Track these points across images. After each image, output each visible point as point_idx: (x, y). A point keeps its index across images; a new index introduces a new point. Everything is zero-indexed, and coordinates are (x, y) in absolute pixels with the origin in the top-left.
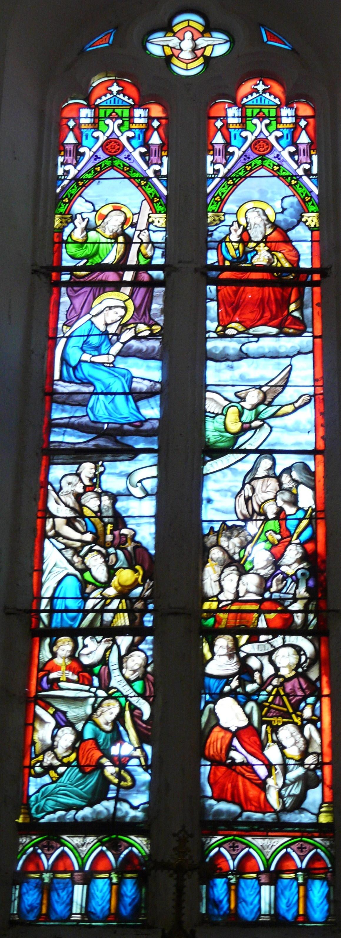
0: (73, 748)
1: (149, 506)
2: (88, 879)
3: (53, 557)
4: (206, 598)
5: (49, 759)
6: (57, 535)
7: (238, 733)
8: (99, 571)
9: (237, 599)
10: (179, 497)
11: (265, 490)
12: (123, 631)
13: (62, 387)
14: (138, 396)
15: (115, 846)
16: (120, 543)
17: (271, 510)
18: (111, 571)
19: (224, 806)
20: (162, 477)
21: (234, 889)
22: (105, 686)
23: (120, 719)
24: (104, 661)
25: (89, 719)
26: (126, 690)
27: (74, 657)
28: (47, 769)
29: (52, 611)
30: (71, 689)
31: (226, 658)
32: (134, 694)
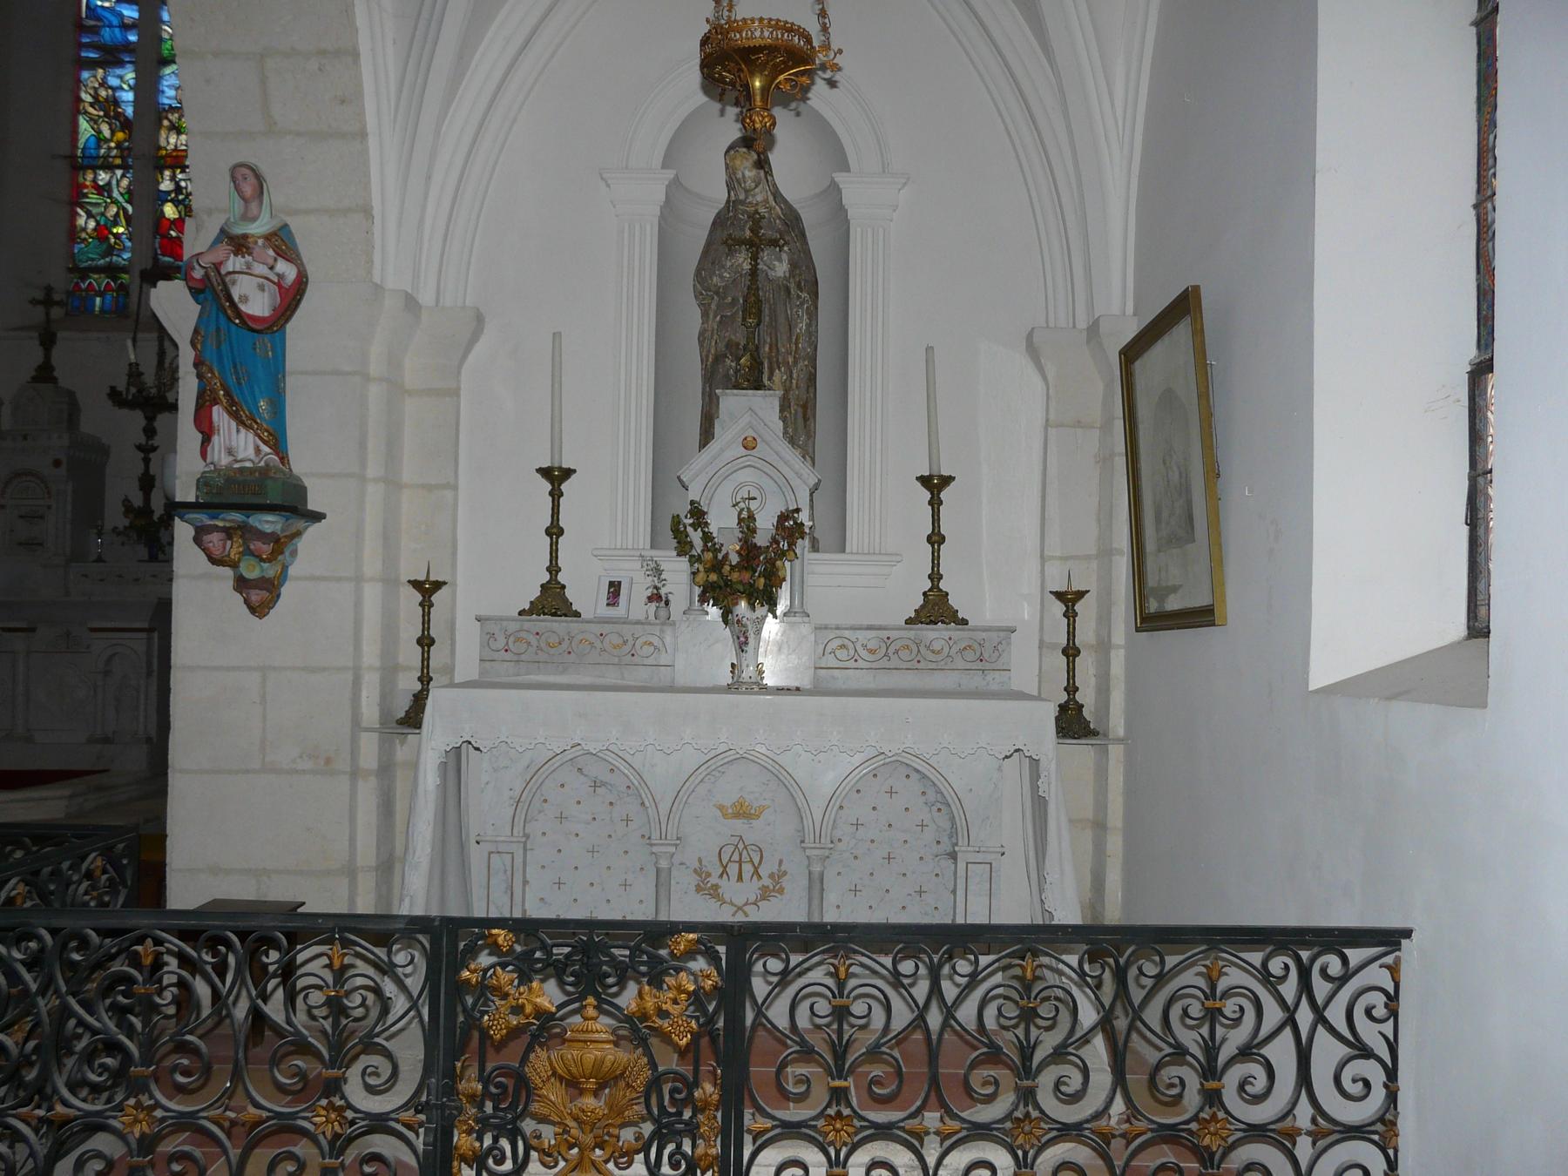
1: (130, 96)
2: (101, 294)
3: (84, 124)
5: (83, 235)
6: (86, 112)
9: (176, 149)
10: (147, 88)
12: (118, 167)
15: (114, 279)
16: (118, 116)
18: (113, 133)
19: (167, 259)
22: (110, 197)
23: (117, 214)
24: (109, 183)
25: (103, 214)
26: (120, 199)
27: (95, 181)
29: (83, 157)
30: (94, 198)
31: (819, 94)
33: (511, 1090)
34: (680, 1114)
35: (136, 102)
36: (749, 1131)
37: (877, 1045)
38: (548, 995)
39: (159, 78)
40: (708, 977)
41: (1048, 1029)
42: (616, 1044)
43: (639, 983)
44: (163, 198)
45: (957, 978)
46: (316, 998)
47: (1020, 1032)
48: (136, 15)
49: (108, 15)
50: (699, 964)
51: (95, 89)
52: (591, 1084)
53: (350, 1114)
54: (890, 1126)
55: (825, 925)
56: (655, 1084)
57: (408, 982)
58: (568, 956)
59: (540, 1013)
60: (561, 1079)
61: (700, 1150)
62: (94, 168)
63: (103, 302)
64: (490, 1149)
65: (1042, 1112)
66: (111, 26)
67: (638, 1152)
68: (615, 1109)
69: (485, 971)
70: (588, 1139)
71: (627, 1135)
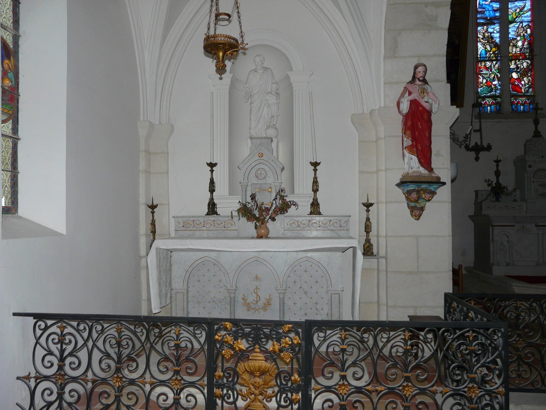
0: (486, 83)
1: (498, 35)
2: (490, 106)
3: (479, 45)
4: (510, 53)
5: (482, 85)
7: (517, 79)
8: (489, 48)
10: (504, 32)
11: (521, 30)
12: (494, 60)
13: (480, 10)
14: (495, 11)
16: (493, 42)
17: (522, 34)
18: (491, 49)
20: (500, 28)
21: (516, 107)
23: (494, 77)
24: (491, 66)
25: (489, 77)
27: (485, 65)
28: (482, 87)
29: (480, 57)
30: (485, 72)
32: (419, 350)
33: (232, 374)
34: (287, 384)
35: (500, 37)
36: (314, 389)
37: (188, 356)
38: (243, 345)
39: (509, 28)
40: (295, 339)
41: (350, 355)
42: (266, 361)
43: (273, 341)
44: (512, 71)
45: (320, 339)
46: (172, 344)
47: (341, 356)
48: (498, 6)
49: (487, 6)
50: (292, 335)
51: (484, 33)
52: (258, 374)
53: (124, 380)
54: (193, 383)
55: (141, 317)
56: (278, 375)
57: (200, 339)
58: (250, 332)
59: (241, 350)
60: (248, 372)
61: (294, 397)
62: (485, 61)
63: (491, 108)
64: (226, 394)
65: (348, 382)
66: (489, 11)
67: (273, 397)
68: (266, 383)
69: (223, 336)
70: (257, 392)
71: (270, 391)
